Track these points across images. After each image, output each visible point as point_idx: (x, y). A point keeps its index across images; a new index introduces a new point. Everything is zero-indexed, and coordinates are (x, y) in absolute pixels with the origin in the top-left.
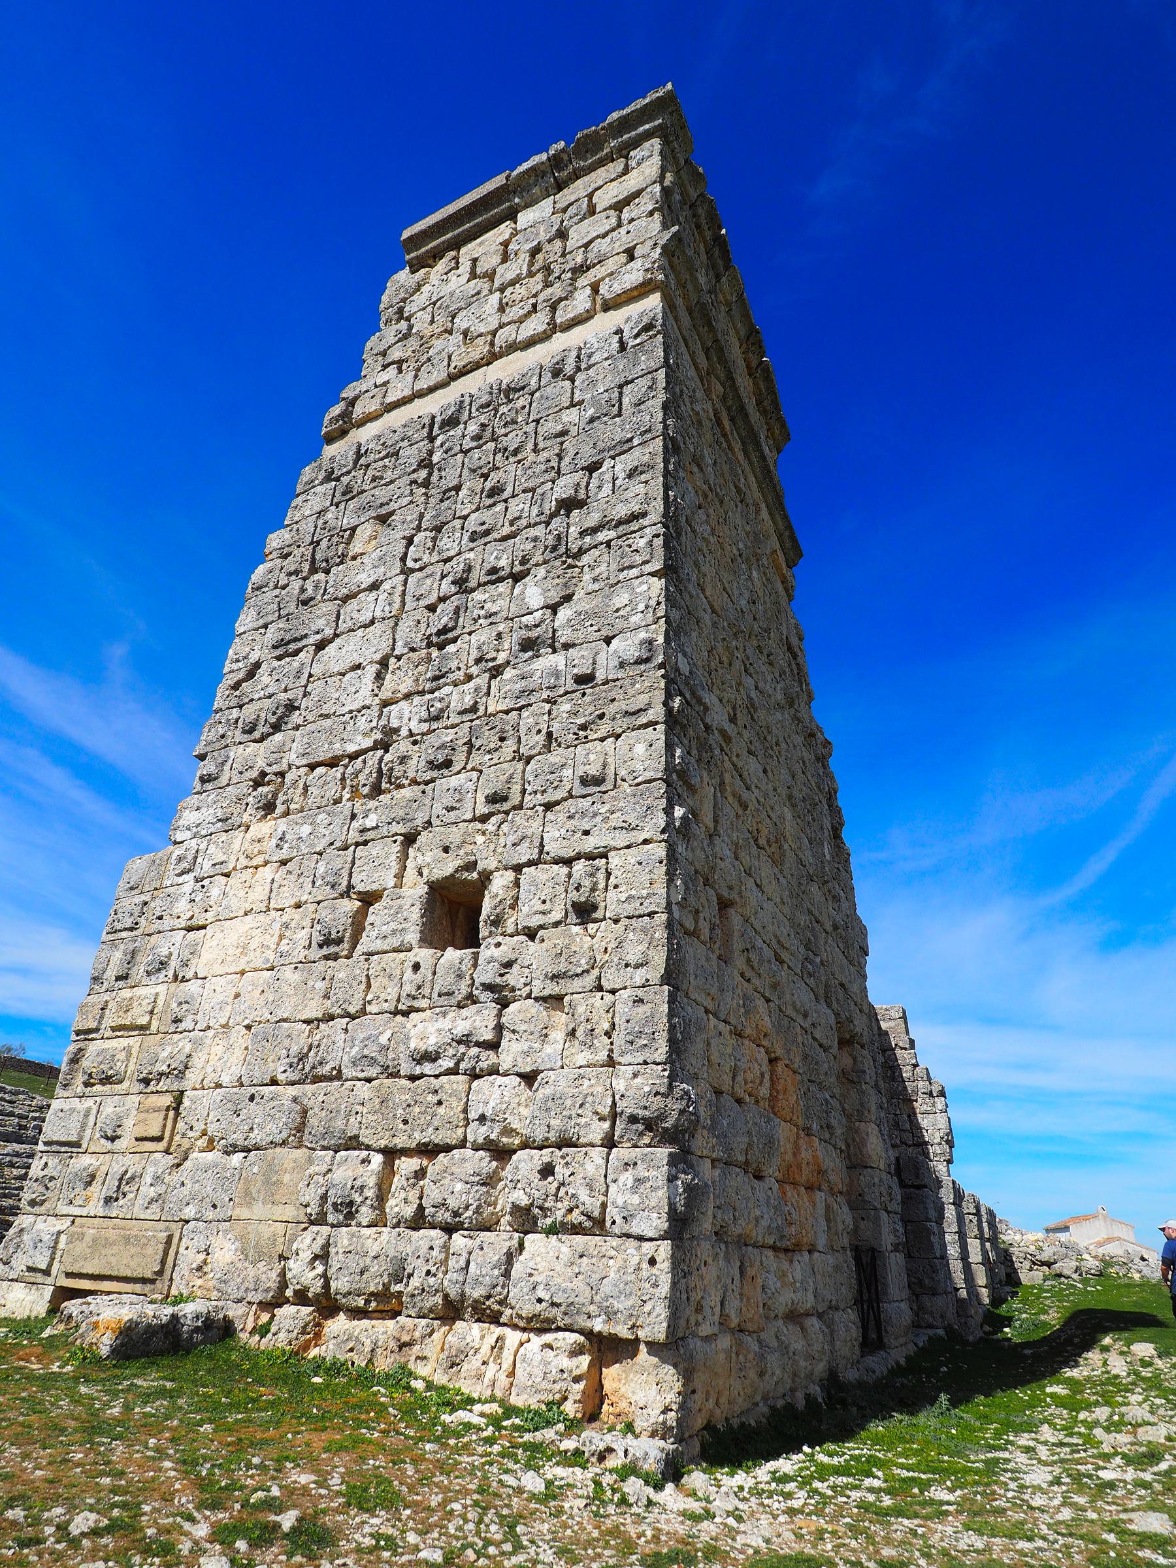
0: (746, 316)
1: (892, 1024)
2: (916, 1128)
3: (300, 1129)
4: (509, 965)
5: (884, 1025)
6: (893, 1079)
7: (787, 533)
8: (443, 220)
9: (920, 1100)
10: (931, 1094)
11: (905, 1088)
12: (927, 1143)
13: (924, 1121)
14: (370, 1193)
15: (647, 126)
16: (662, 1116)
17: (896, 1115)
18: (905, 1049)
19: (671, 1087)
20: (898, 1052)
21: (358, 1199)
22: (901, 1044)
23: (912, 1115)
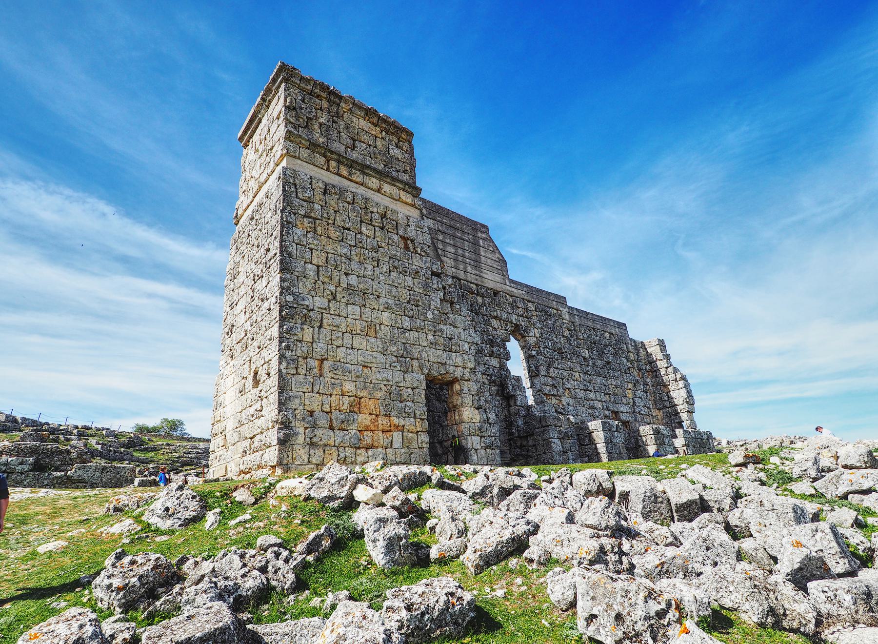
0: (360, 107)
1: (653, 348)
2: (670, 398)
3: (823, 471)
4: (261, 391)
5: (649, 350)
6: (656, 376)
7: (407, 187)
8: (244, 131)
9: (671, 384)
10: (676, 380)
11: (663, 380)
12: (676, 405)
13: (673, 394)
14: (248, 448)
15: (280, 79)
16: (278, 420)
17: (660, 394)
18: (661, 360)
19: (279, 413)
20: (658, 362)
21: (246, 449)
22: (659, 358)
23: (668, 393)
